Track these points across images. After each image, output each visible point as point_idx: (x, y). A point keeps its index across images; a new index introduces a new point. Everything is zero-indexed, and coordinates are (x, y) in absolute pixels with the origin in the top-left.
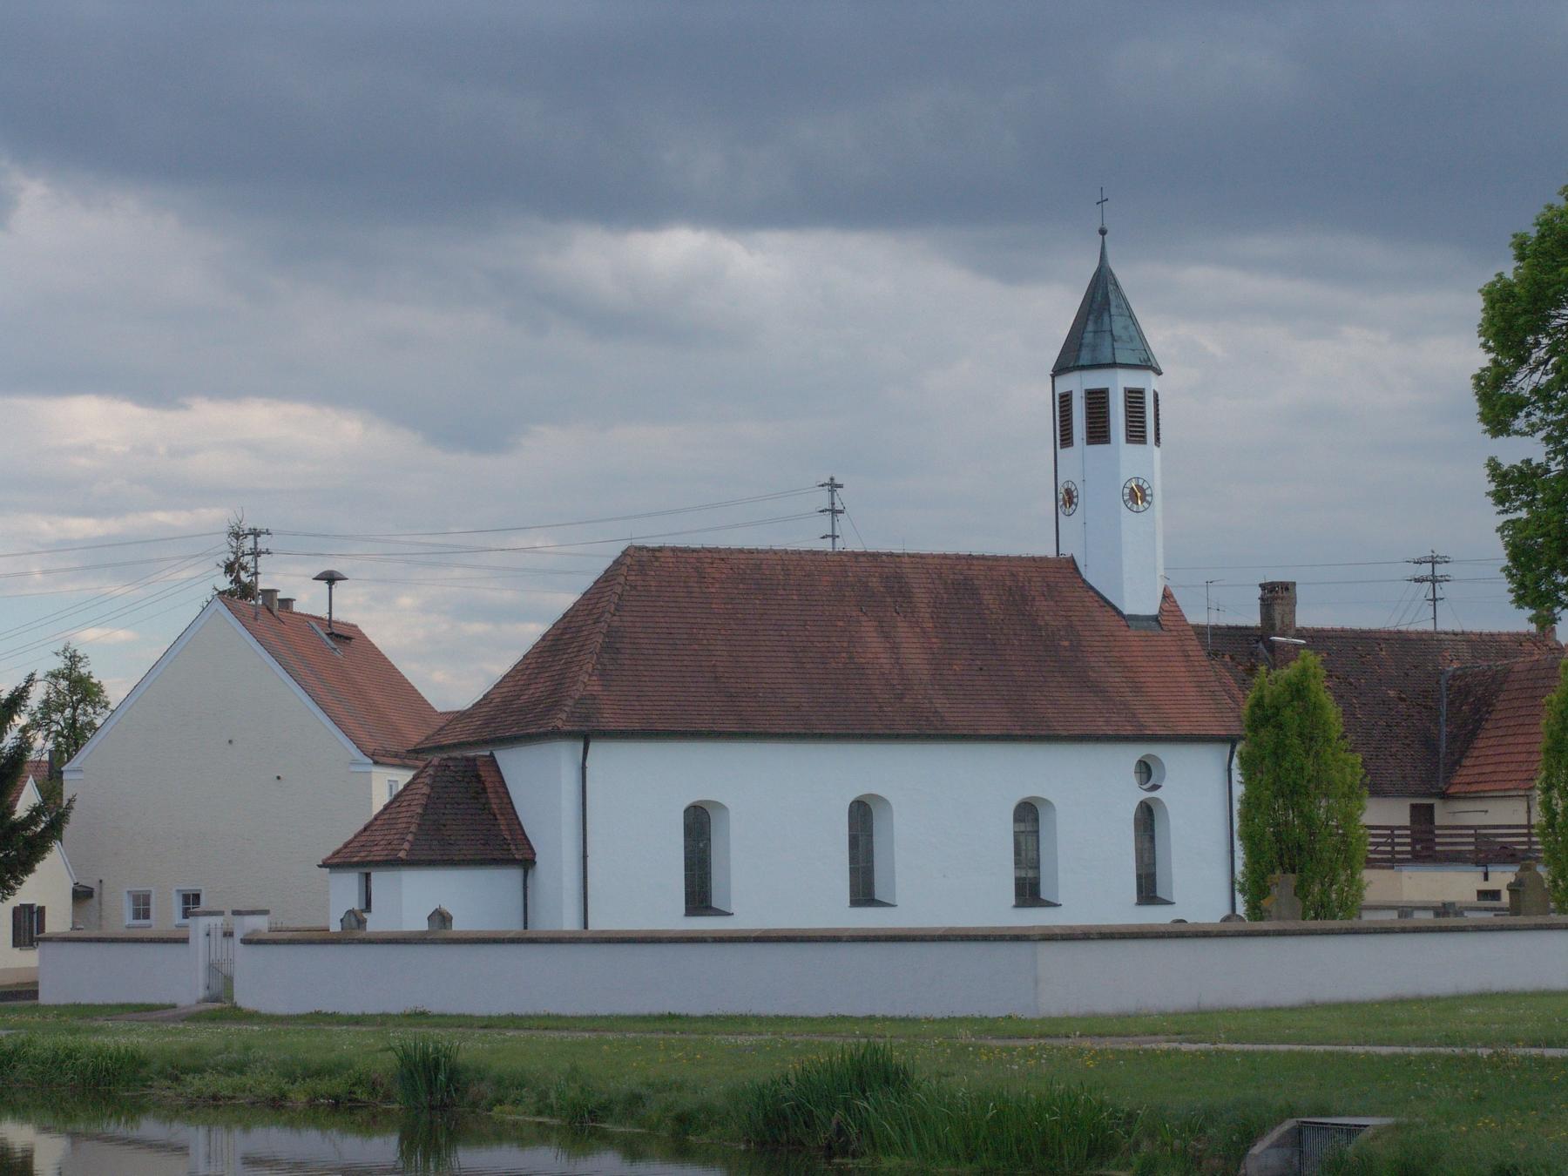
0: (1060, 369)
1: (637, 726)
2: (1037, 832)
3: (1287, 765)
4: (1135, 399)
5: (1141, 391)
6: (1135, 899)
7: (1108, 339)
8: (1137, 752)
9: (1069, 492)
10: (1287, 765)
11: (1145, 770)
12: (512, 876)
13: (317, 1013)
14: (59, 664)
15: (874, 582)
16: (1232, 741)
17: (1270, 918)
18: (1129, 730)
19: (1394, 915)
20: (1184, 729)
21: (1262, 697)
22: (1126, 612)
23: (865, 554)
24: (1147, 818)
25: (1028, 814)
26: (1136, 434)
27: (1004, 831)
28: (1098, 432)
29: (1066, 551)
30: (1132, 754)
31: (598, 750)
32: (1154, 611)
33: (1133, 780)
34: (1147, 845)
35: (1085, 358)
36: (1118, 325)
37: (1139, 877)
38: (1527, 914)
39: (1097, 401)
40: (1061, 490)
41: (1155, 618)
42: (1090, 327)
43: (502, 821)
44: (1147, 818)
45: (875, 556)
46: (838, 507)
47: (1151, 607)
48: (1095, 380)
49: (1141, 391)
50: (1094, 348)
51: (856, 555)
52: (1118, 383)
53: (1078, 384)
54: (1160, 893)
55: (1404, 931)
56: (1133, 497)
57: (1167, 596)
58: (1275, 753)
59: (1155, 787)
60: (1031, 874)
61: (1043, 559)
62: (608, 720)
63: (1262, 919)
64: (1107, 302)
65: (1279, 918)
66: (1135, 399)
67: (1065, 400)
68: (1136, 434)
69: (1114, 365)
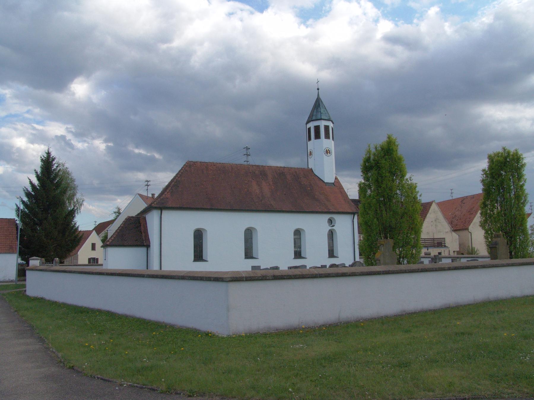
0: (308, 122)
1: (178, 206)
2: (300, 238)
3: (384, 186)
4: (327, 128)
5: (328, 126)
6: (328, 256)
7: (319, 114)
8: (328, 216)
9: (310, 152)
10: (384, 186)
11: (330, 221)
12: (143, 250)
13: (42, 298)
14: (116, 210)
15: (257, 172)
16: (354, 214)
17: (380, 264)
18: (326, 210)
19: (449, 261)
20: (341, 210)
21: (369, 158)
22: (325, 181)
23: (255, 165)
24: (331, 235)
25: (298, 233)
26: (327, 136)
27: (291, 238)
28: (317, 136)
29: (310, 167)
30: (327, 217)
31: (165, 213)
32: (333, 182)
33: (327, 224)
34: (331, 242)
35: (314, 118)
36: (322, 110)
37: (329, 250)
38: (500, 259)
39: (317, 128)
40: (309, 152)
41: (333, 183)
42: (315, 111)
43: (143, 234)
44: (331, 235)
45: (258, 166)
46: (248, 154)
47: (332, 181)
48: (316, 123)
49: (328, 126)
50: (316, 116)
51: (253, 166)
52: (322, 124)
53: (312, 125)
54: (335, 255)
55: (456, 268)
56: (327, 152)
57: (336, 178)
58: (377, 181)
59: (333, 226)
60: (299, 250)
61: (304, 169)
62: (170, 204)
63: (372, 265)
64: (319, 105)
65: (385, 264)
66: (327, 128)
67: (309, 129)
68: (327, 136)
69: (321, 119)
